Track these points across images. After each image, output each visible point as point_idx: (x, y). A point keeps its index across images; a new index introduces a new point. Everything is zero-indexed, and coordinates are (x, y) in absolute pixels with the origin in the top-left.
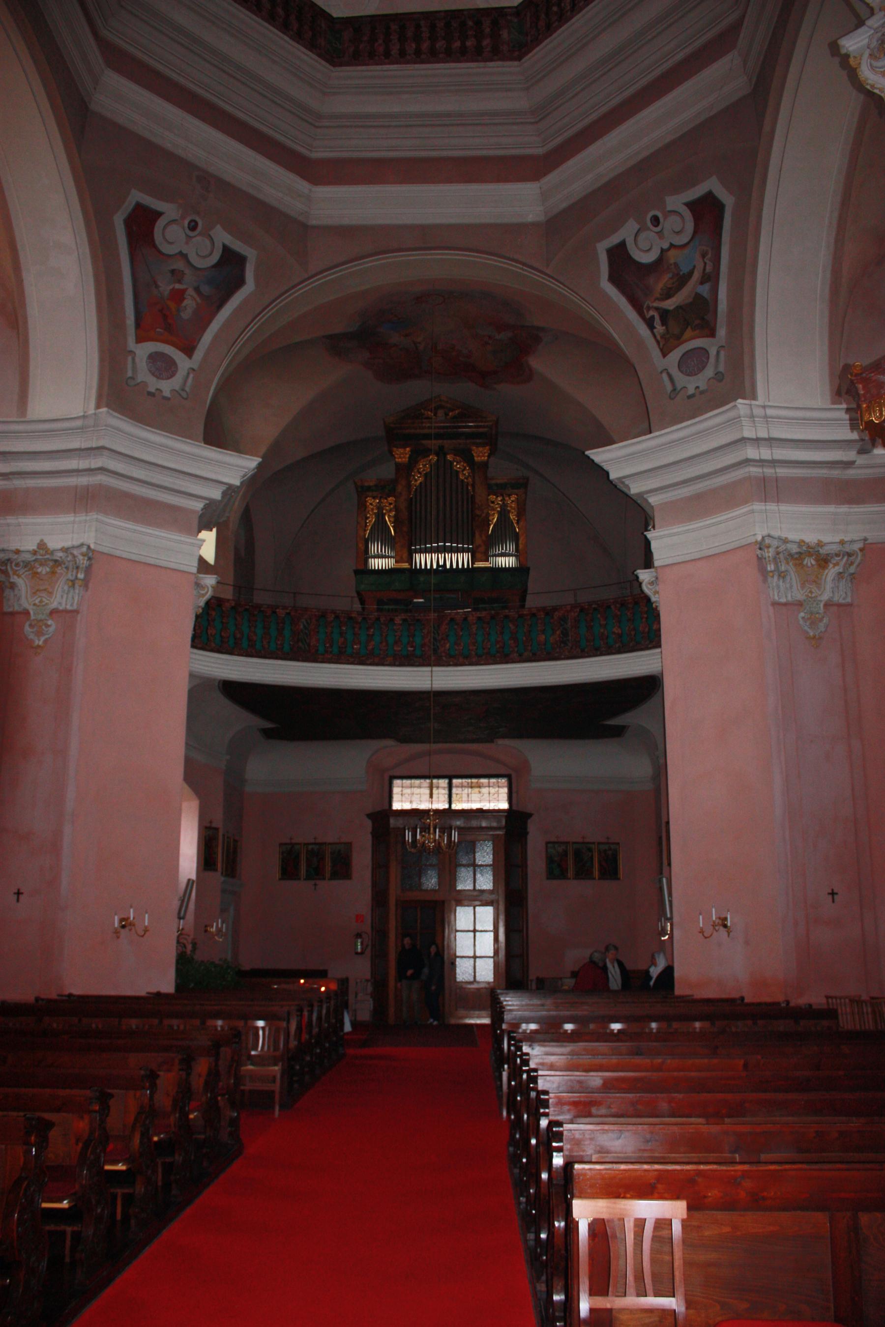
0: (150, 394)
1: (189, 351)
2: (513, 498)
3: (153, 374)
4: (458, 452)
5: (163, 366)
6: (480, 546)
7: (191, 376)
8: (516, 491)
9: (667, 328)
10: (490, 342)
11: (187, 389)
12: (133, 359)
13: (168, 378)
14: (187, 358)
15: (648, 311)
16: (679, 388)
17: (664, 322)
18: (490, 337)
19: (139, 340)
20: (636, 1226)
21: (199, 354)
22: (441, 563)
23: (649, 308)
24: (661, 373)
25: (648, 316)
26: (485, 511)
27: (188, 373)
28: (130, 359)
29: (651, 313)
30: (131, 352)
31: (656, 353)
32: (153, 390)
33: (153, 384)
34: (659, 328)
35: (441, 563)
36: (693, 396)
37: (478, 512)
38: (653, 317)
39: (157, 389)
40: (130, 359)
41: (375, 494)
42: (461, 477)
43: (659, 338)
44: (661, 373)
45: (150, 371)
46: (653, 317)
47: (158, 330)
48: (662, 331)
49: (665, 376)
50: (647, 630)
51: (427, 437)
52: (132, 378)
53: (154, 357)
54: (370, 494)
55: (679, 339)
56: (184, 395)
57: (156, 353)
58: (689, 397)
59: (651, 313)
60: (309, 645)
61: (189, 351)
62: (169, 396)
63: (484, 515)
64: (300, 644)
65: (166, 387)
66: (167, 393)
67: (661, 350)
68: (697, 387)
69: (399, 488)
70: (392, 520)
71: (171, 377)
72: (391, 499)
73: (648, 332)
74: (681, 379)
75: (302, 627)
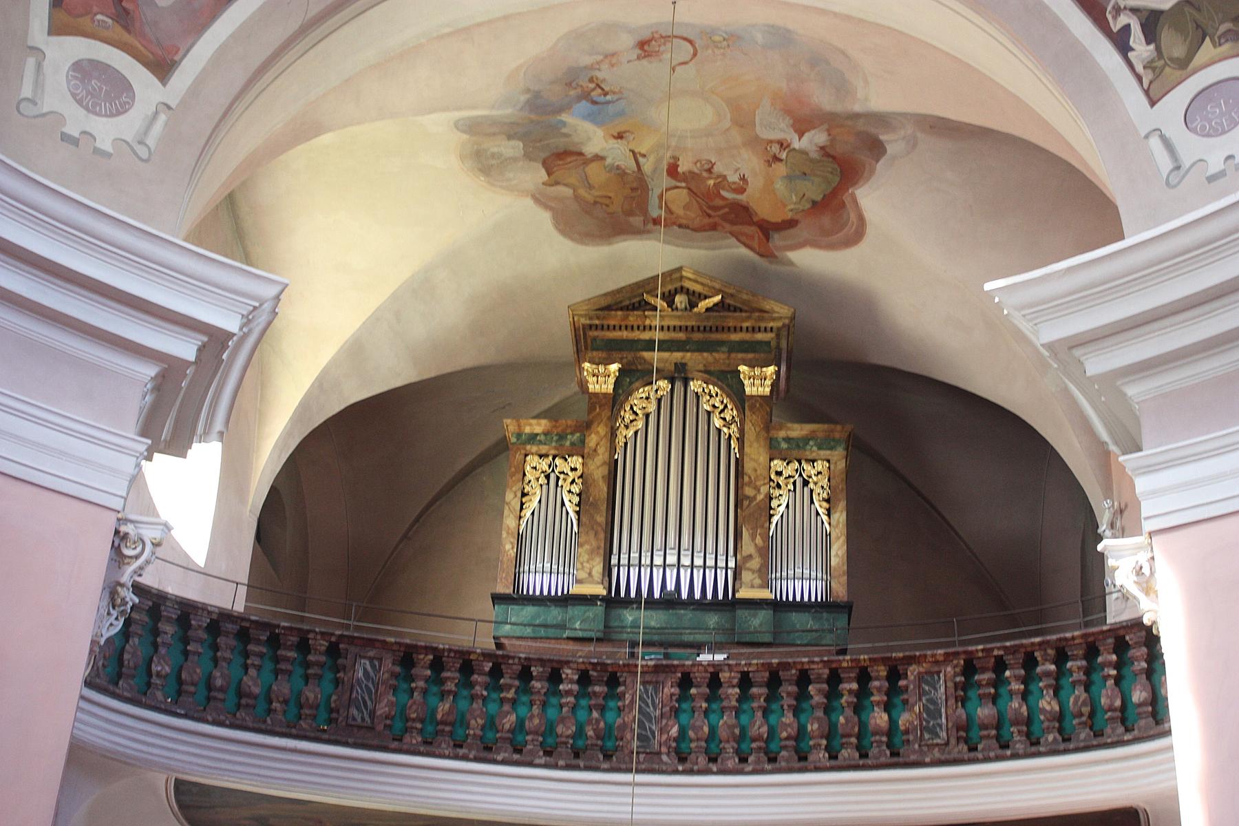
0: (65, 138)
1: (162, 67)
2: (820, 465)
3: (79, 102)
4: (711, 375)
5: (106, 92)
6: (750, 557)
7: (162, 118)
8: (825, 453)
9: (1158, 49)
10: (784, 155)
11: (151, 142)
12: (39, 66)
13: (112, 115)
14: (159, 84)
15: (1115, 18)
16: (1186, 163)
17: (1150, 35)
18: (782, 144)
19: (56, 29)
20: (497, 444)
21: (184, 77)
22: (671, 586)
23: (1118, 10)
24: (1147, 137)
25: (1116, 26)
26: (764, 490)
27: (157, 113)
28: (31, 62)
29: (1123, 19)
30: (35, 50)
31: (1131, 95)
32: (76, 135)
33: (77, 120)
34: (1141, 49)
35: (671, 586)
36: (1222, 174)
37: (749, 491)
38: (1127, 29)
39: (84, 133)
40: (31, 62)
41: (544, 449)
42: (718, 423)
43: (1139, 68)
44: (1147, 137)
45: (74, 95)
46: (1127, 29)
47: (99, 17)
48: (1145, 55)
49: (1155, 143)
50: (1118, 703)
51: (649, 345)
52: (33, 102)
53: (84, 70)
54: (534, 449)
55: (1184, 65)
56: (143, 152)
57: (91, 61)
58: (1211, 179)
59: (1123, 19)
60: (372, 714)
61: (162, 67)
62: (111, 151)
63: (760, 497)
64: (354, 711)
65: (107, 131)
66: (106, 144)
67: (1147, 92)
68: (1230, 157)
69: (592, 440)
70: (576, 499)
71: (119, 113)
72: (576, 461)
73: (1116, 58)
74: (1190, 146)
75: (361, 674)
